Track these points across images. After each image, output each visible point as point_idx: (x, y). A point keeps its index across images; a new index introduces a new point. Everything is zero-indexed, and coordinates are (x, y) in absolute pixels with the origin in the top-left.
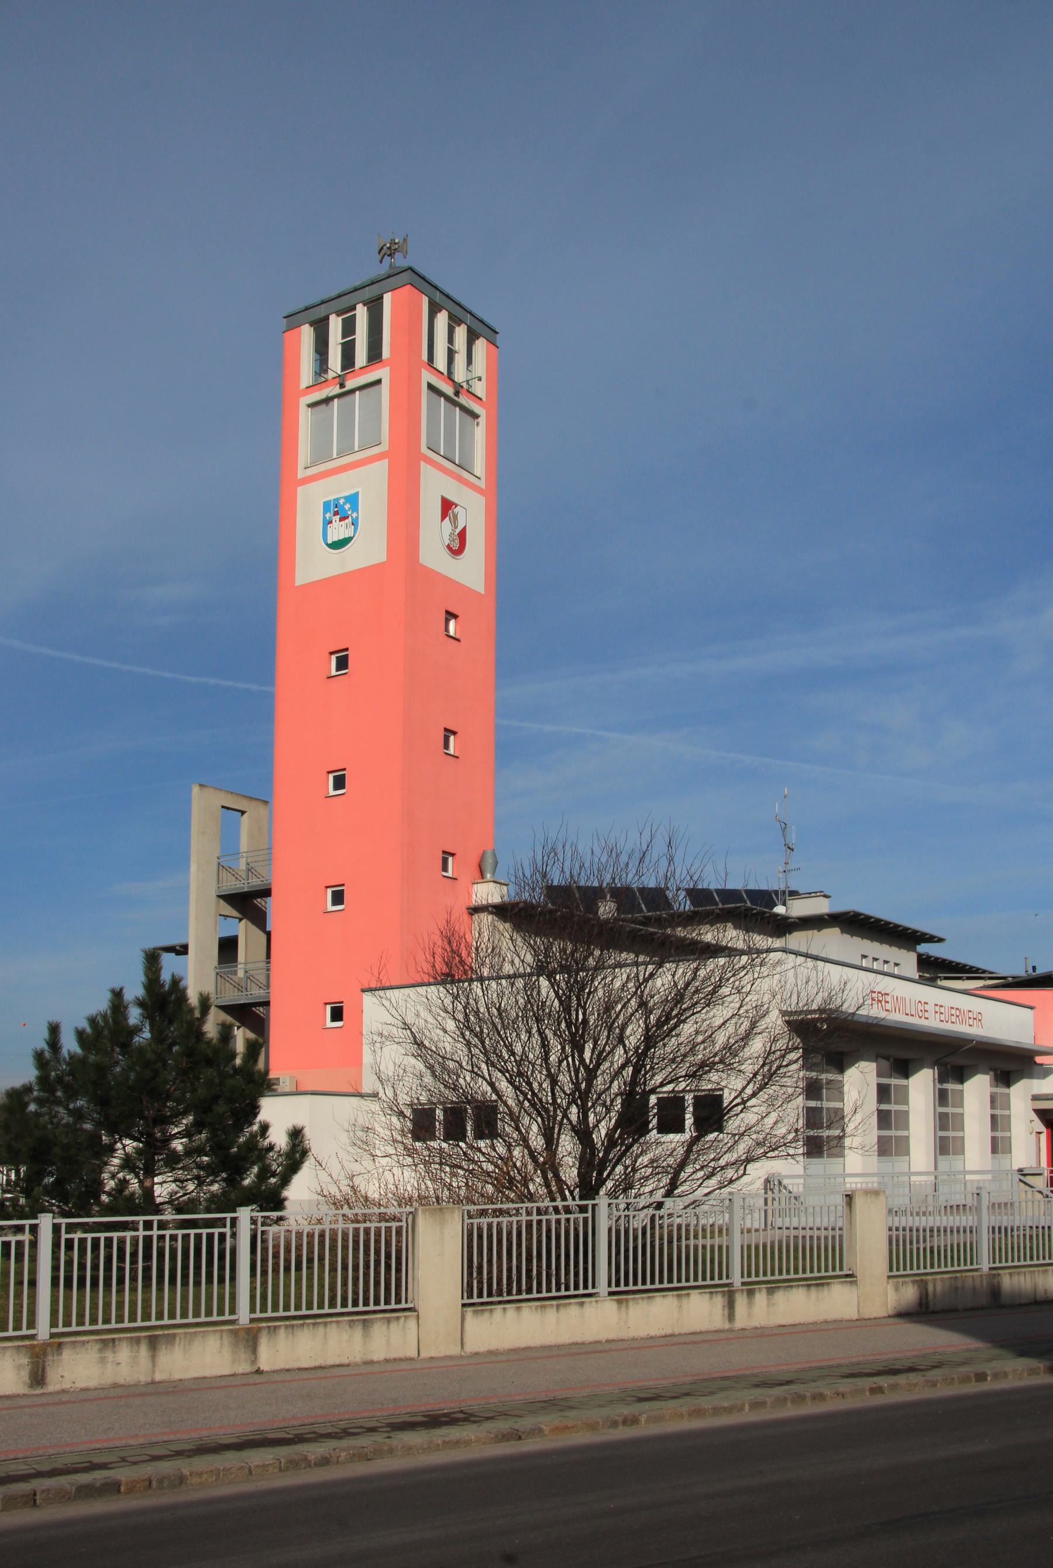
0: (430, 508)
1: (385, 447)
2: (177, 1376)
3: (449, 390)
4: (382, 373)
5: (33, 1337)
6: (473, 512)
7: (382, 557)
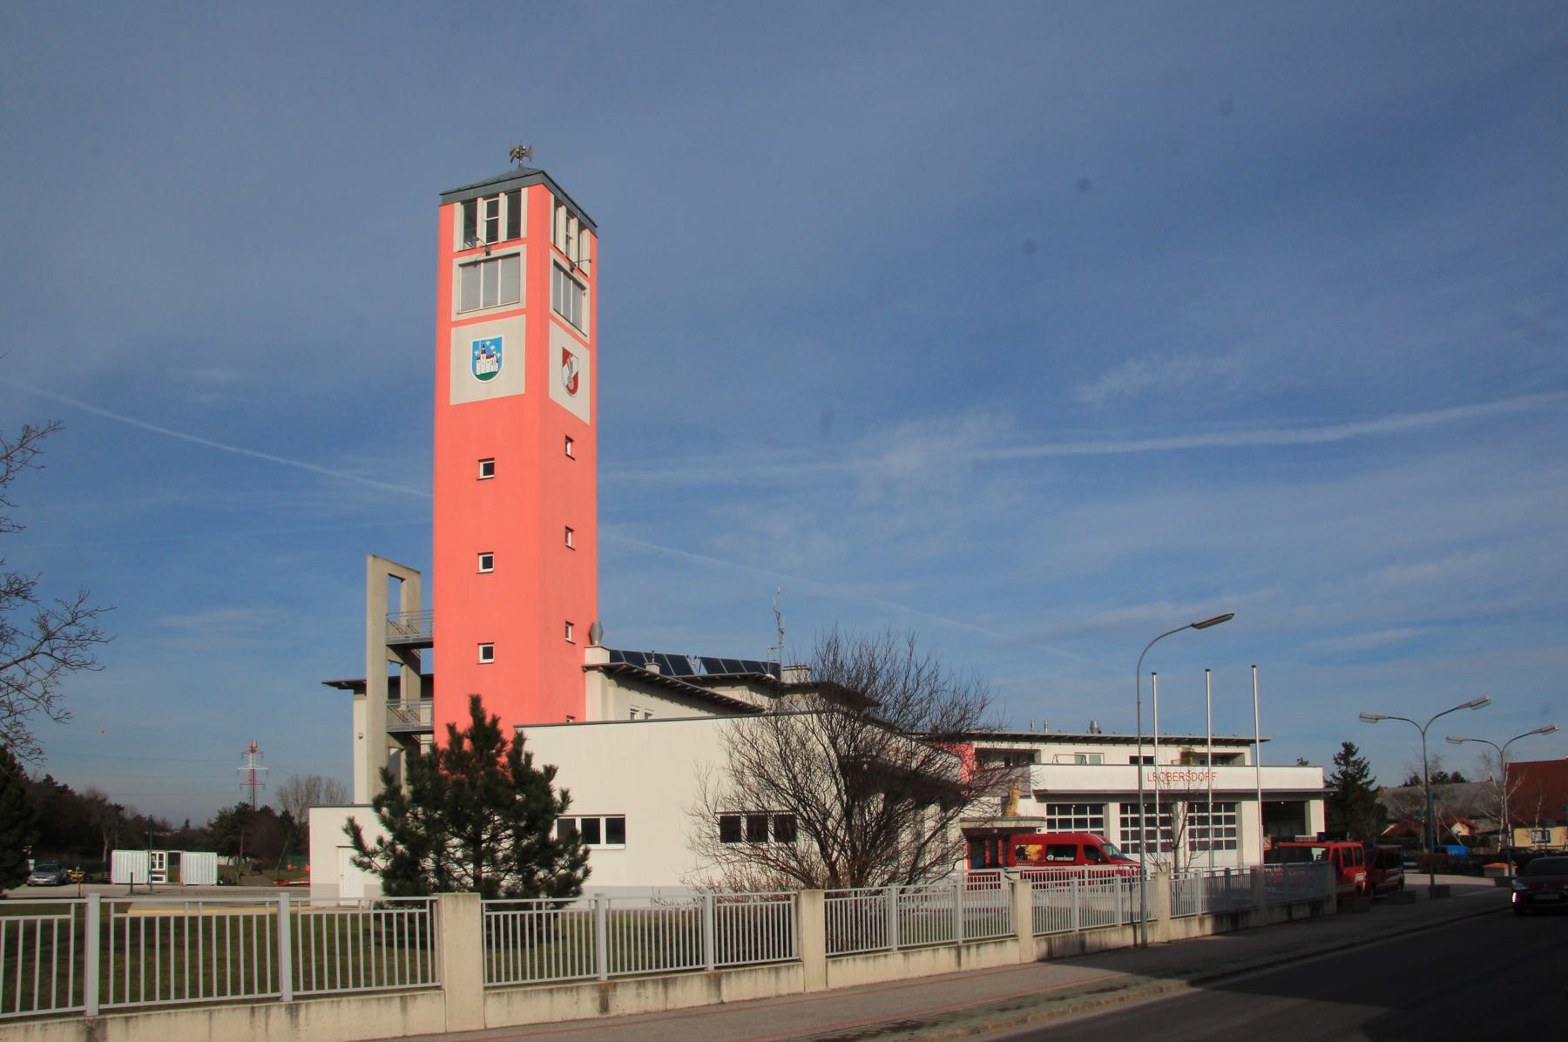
0: (556, 357)
1: (523, 305)
2: (680, 1006)
3: (567, 267)
4: (521, 248)
5: (81, 1013)
6: (583, 362)
7: (522, 391)
